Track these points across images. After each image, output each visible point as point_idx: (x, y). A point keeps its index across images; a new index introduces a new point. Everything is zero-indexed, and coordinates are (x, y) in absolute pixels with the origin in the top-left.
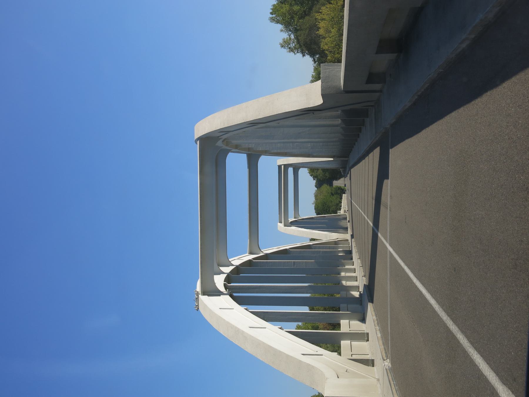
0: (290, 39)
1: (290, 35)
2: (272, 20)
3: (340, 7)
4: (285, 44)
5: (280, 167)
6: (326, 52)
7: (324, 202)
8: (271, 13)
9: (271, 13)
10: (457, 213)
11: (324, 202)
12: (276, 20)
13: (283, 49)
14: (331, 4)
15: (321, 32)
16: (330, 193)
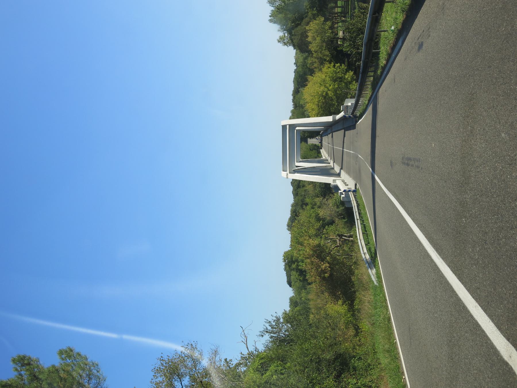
0: (285, 36)
1: (285, 33)
2: (271, 21)
3: (322, 22)
4: (281, 40)
5: (284, 127)
6: (313, 52)
7: (305, 155)
8: (270, 16)
9: (270, 16)
10: (468, 188)
11: (305, 155)
12: (273, 21)
13: (279, 43)
14: (316, 20)
15: (309, 39)
16: (309, 149)
